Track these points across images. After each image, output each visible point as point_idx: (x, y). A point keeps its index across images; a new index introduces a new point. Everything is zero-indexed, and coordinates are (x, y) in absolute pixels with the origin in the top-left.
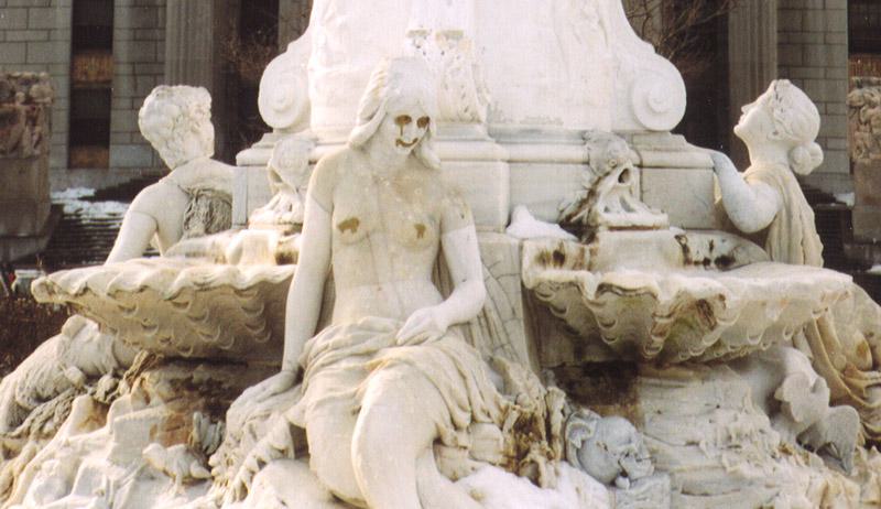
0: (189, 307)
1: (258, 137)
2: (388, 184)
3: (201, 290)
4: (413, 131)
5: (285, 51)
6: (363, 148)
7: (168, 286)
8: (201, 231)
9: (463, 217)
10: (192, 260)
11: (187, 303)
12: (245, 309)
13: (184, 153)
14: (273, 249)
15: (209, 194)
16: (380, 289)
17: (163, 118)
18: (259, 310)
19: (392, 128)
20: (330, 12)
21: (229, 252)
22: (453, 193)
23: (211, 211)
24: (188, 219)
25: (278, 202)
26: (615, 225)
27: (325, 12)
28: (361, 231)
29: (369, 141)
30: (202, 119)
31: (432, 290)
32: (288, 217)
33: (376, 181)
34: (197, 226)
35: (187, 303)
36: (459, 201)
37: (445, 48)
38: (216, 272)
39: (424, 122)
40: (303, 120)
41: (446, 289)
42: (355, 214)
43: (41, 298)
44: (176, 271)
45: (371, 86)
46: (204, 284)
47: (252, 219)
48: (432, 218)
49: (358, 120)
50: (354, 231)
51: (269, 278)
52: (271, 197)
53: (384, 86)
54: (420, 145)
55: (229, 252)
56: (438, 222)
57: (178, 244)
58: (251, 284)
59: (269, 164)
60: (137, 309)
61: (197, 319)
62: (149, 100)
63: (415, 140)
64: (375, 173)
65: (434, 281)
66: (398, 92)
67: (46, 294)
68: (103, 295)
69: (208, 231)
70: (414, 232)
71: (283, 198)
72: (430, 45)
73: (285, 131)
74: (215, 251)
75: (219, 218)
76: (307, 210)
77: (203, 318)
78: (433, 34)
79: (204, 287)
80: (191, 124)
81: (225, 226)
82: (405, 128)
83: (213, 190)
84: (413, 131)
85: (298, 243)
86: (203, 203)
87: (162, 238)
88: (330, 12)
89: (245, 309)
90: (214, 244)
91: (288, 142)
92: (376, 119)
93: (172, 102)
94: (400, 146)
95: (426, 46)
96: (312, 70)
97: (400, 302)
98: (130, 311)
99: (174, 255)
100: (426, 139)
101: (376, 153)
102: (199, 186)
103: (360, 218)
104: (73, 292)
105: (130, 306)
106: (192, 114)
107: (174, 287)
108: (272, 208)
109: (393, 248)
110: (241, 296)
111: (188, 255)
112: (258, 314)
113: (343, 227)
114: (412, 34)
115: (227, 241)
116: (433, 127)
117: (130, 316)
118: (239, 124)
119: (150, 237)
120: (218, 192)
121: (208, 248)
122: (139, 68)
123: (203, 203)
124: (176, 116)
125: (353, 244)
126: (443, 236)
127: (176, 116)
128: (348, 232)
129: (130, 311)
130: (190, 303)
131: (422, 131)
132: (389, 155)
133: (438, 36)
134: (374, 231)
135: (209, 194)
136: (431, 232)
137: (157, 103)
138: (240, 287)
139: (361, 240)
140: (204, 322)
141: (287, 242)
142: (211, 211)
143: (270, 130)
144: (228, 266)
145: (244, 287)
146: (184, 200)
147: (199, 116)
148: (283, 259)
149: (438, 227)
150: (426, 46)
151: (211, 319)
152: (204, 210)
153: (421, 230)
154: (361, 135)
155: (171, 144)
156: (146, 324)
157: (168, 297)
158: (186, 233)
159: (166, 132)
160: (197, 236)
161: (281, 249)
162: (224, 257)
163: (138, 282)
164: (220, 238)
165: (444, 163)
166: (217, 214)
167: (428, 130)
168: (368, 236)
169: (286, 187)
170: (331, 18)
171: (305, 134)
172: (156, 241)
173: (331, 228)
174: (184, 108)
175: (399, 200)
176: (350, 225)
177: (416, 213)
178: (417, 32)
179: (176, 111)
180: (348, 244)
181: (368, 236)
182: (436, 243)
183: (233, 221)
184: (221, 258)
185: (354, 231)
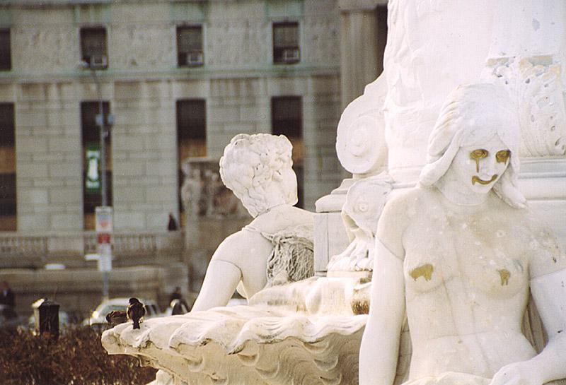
0: (257, 360)
1: (337, 183)
2: (465, 226)
3: (266, 343)
4: (491, 166)
5: (363, 94)
6: (436, 187)
7: (233, 338)
8: (285, 279)
9: (555, 261)
10: (274, 308)
11: (254, 357)
12: (319, 362)
13: (266, 201)
14: (350, 297)
15: (291, 241)
16: (460, 342)
17: (242, 166)
18: (333, 362)
19: (466, 163)
20: (404, 47)
21: (308, 300)
22: (542, 234)
23: (295, 258)
24: (272, 268)
25: (355, 248)
26: (123, 78)
27: (398, 48)
28: (436, 278)
29: (442, 179)
30: (282, 167)
31: (521, 342)
32: (363, 263)
33: (452, 223)
34: (281, 273)
35: (254, 357)
36: (549, 243)
37: (532, 76)
38: (284, 322)
39: (504, 155)
40: (382, 163)
41: (539, 337)
42: (430, 260)
43: (111, 349)
44: (251, 320)
45: (442, 118)
46: (268, 337)
47: (330, 267)
48: (518, 262)
49: (429, 158)
50: (428, 277)
51: (340, 329)
52: (348, 244)
53: (456, 117)
54: (500, 182)
55: (308, 300)
56: (525, 267)
57: (263, 291)
58: (320, 336)
59: (343, 209)
60: (203, 362)
61: (267, 373)
62: (228, 149)
63: (495, 177)
64: (450, 214)
65: (524, 331)
66: (472, 123)
67: (115, 345)
68: (166, 348)
69: (291, 279)
70: (497, 278)
71: (360, 244)
72: (513, 73)
73: (364, 175)
74: (296, 299)
75: (302, 265)
76: (379, 258)
77: (274, 371)
78: (517, 60)
79: (269, 340)
80: (271, 171)
81: (308, 274)
82: (482, 164)
83: (296, 238)
84: (491, 166)
85: (371, 293)
86: (286, 250)
87: (247, 285)
88: (404, 47)
89: (319, 362)
90: (294, 292)
91: (365, 184)
92: (449, 154)
93: (251, 150)
94: (477, 183)
95: (508, 74)
96: (386, 110)
97: (485, 357)
98: (196, 364)
99: (257, 303)
100: (507, 176)
101: (450, 193)
102: (281, 233)
103: (434, 265)
104: (136, 344)
105: (197, 360)
106: (272, 162)
107: (238, 341)
108: (349, 255)
109: (473, 296)
110: (312, 348)
111: (270, 303)
112: (333, 366)
113: (415, 274)
114: (492, 63)
115: (307, 289)
116: (515, 160)
117: (198, 370)
118: (319, 172)
119: (236, 284)
120: (301, 240)
121: (289, 297)
122: (323, 151)
123: (286, 250)
124: (255, 163)
125: (427, 292)
126: (533, 282)
127: (255, 163)
128: (421, 279)
129: (196, 364)
130: (258, 357)
131: (503, 166)
132: (465, 195)
133: (522, 63)
134: (452, 277)
135: (291, 241)
136: (517, 278)
137: (235, 152)
138: (308, 340)
139: (436, 288)
140: (275, 375)
141: (362, 290)
142: (295, 258)
143: (350, 175)
144: (300, 315)
145: (313, 339)
146: (268, 247)
147: (280, 164)
148: (361, 309)
149: (525, 272)
150: (508, 74)
151: (281, 371)
152: (287, 258)
153: (505, 276)
154: (432, 174)
155: (252, 193)
156: (215, 377)
157: (232, 351)
158: (270, 281)
159: (247, 180)
160: (280, 283)
161: (358, 297)
162: (305, 306)
163: (201, 335)
164: (298, 285)
165: (530, 202)
166: (301, 263)
167: (510, 164)
168: (444, 283)
169: (363, 233)
170: (405, 53)
171: (381, 177)
172: (241, 289)
173: (404, 279)
174: (263, 155)
175: (478, 243)
176: (423, 271)
177: (500, 257)
178: (499, 60)
179: (255, 159)
180: (421, 292)
181: (444, 283)
182: (525, 290)
183: (315, 268)
184: (301, 306)
185: (428, 277)
